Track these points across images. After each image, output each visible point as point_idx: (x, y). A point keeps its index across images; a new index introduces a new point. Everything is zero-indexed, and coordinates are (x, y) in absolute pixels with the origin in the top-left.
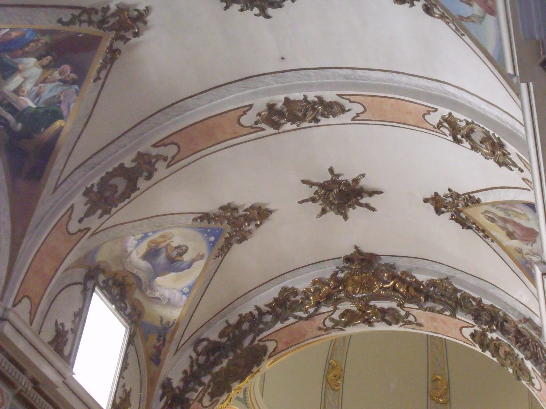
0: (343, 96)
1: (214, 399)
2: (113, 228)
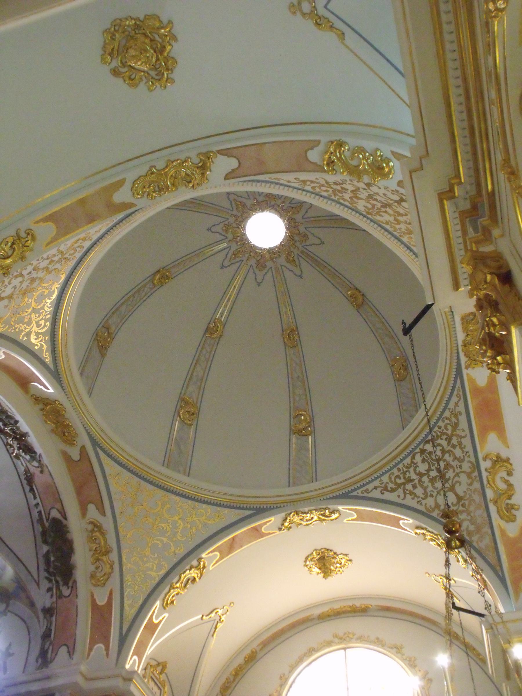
0: (98, 449)
1: (70, 584)
2: (203, 399)
